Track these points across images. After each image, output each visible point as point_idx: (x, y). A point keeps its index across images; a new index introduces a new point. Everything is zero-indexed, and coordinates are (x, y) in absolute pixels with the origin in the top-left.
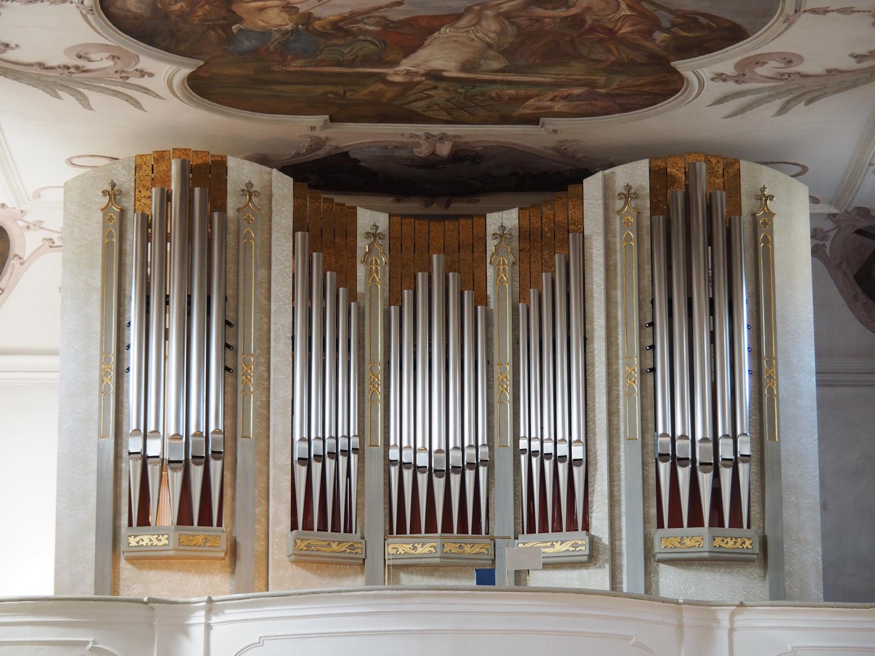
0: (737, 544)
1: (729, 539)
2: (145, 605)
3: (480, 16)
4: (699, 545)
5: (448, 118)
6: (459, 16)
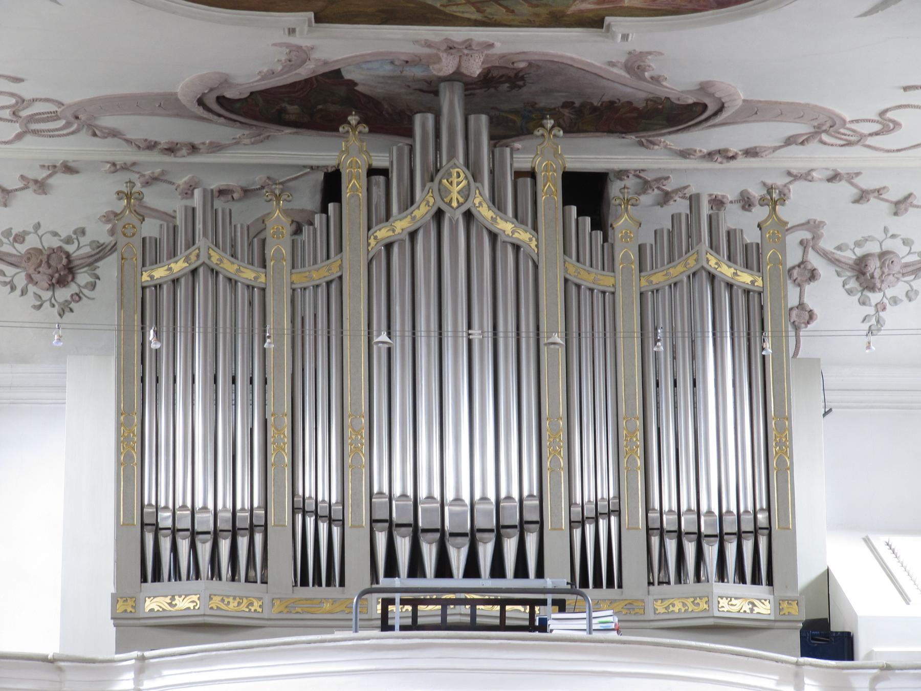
0: (242, 605)
1: (231, 599)
2: (50, 664)
4: (194, 607)
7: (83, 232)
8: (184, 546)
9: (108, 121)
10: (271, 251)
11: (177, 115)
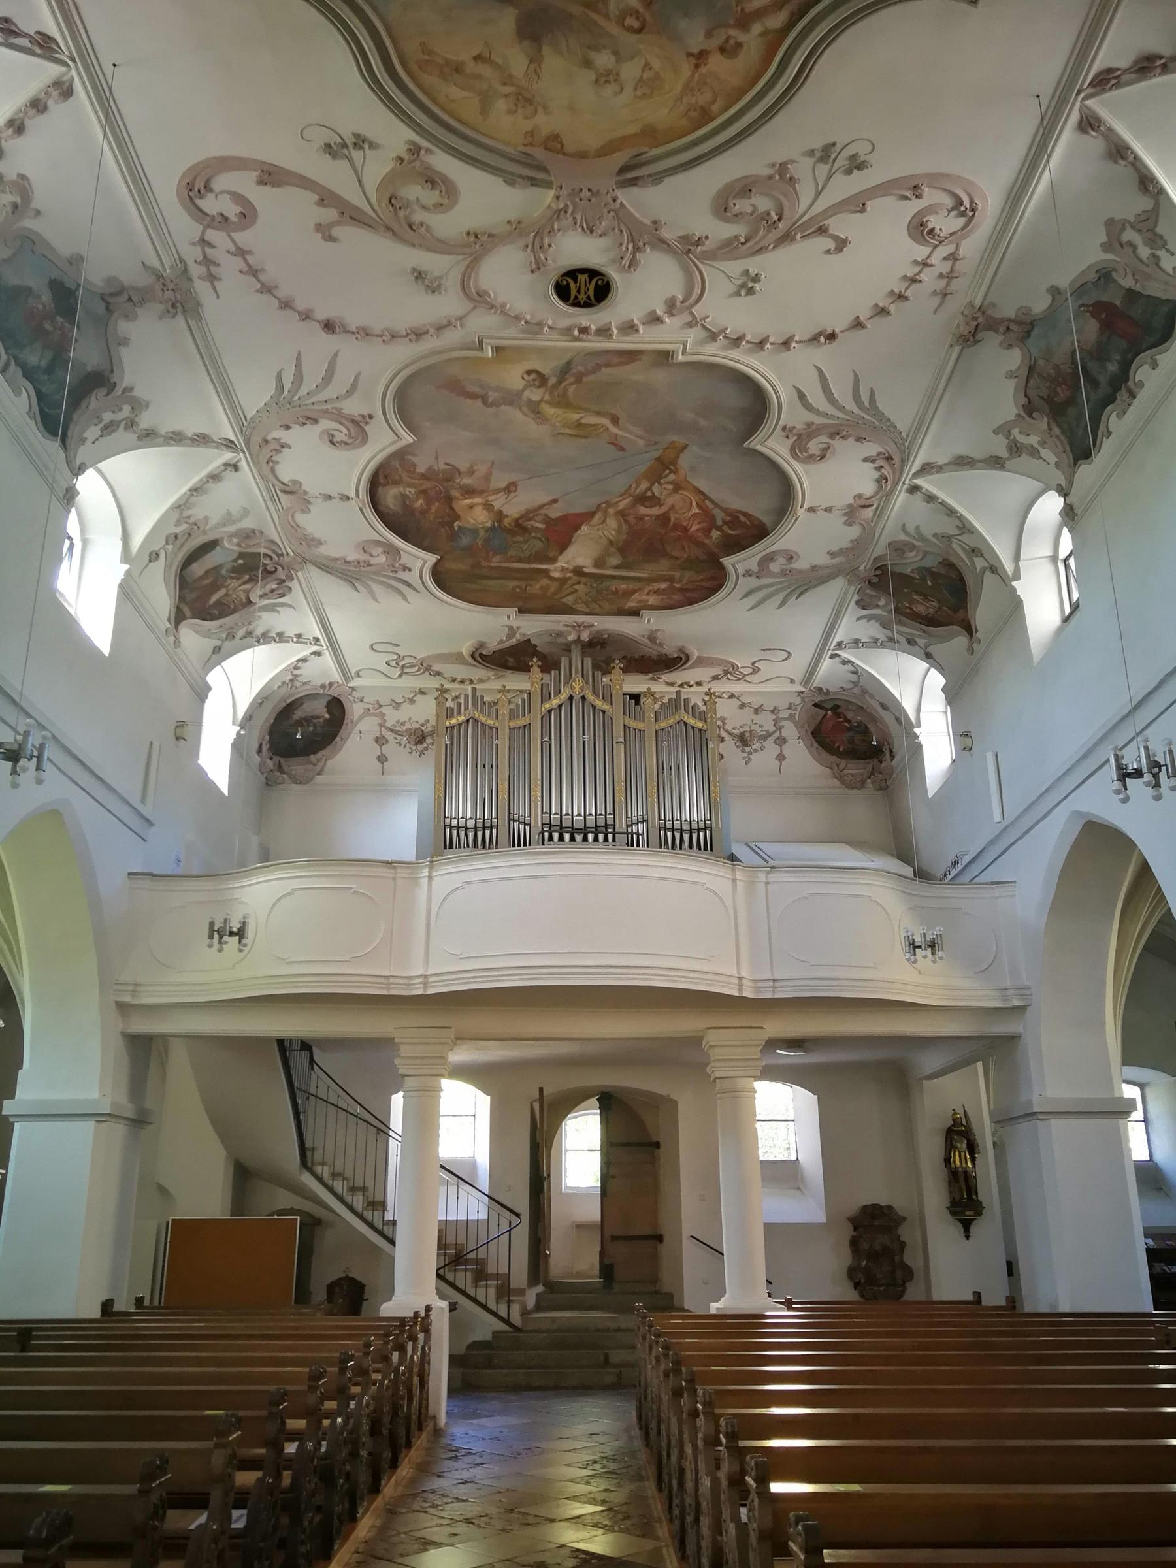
3: (606, 515)
5: (587, 610)
6: (592, 514)
7: (428, 721)
8: (462, 833)
9: (437, 667)
10: (500, 713)
11: (464, 664)
